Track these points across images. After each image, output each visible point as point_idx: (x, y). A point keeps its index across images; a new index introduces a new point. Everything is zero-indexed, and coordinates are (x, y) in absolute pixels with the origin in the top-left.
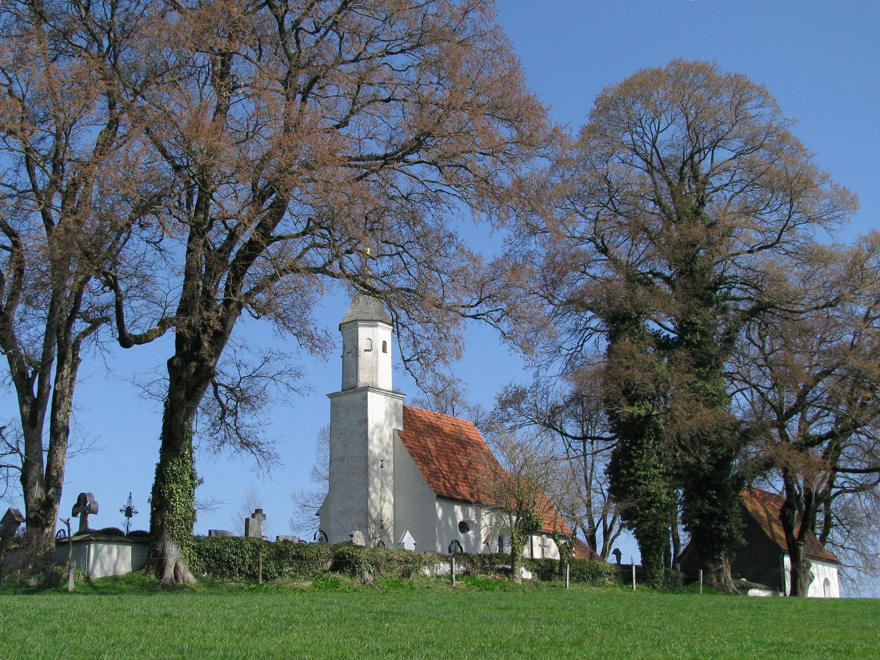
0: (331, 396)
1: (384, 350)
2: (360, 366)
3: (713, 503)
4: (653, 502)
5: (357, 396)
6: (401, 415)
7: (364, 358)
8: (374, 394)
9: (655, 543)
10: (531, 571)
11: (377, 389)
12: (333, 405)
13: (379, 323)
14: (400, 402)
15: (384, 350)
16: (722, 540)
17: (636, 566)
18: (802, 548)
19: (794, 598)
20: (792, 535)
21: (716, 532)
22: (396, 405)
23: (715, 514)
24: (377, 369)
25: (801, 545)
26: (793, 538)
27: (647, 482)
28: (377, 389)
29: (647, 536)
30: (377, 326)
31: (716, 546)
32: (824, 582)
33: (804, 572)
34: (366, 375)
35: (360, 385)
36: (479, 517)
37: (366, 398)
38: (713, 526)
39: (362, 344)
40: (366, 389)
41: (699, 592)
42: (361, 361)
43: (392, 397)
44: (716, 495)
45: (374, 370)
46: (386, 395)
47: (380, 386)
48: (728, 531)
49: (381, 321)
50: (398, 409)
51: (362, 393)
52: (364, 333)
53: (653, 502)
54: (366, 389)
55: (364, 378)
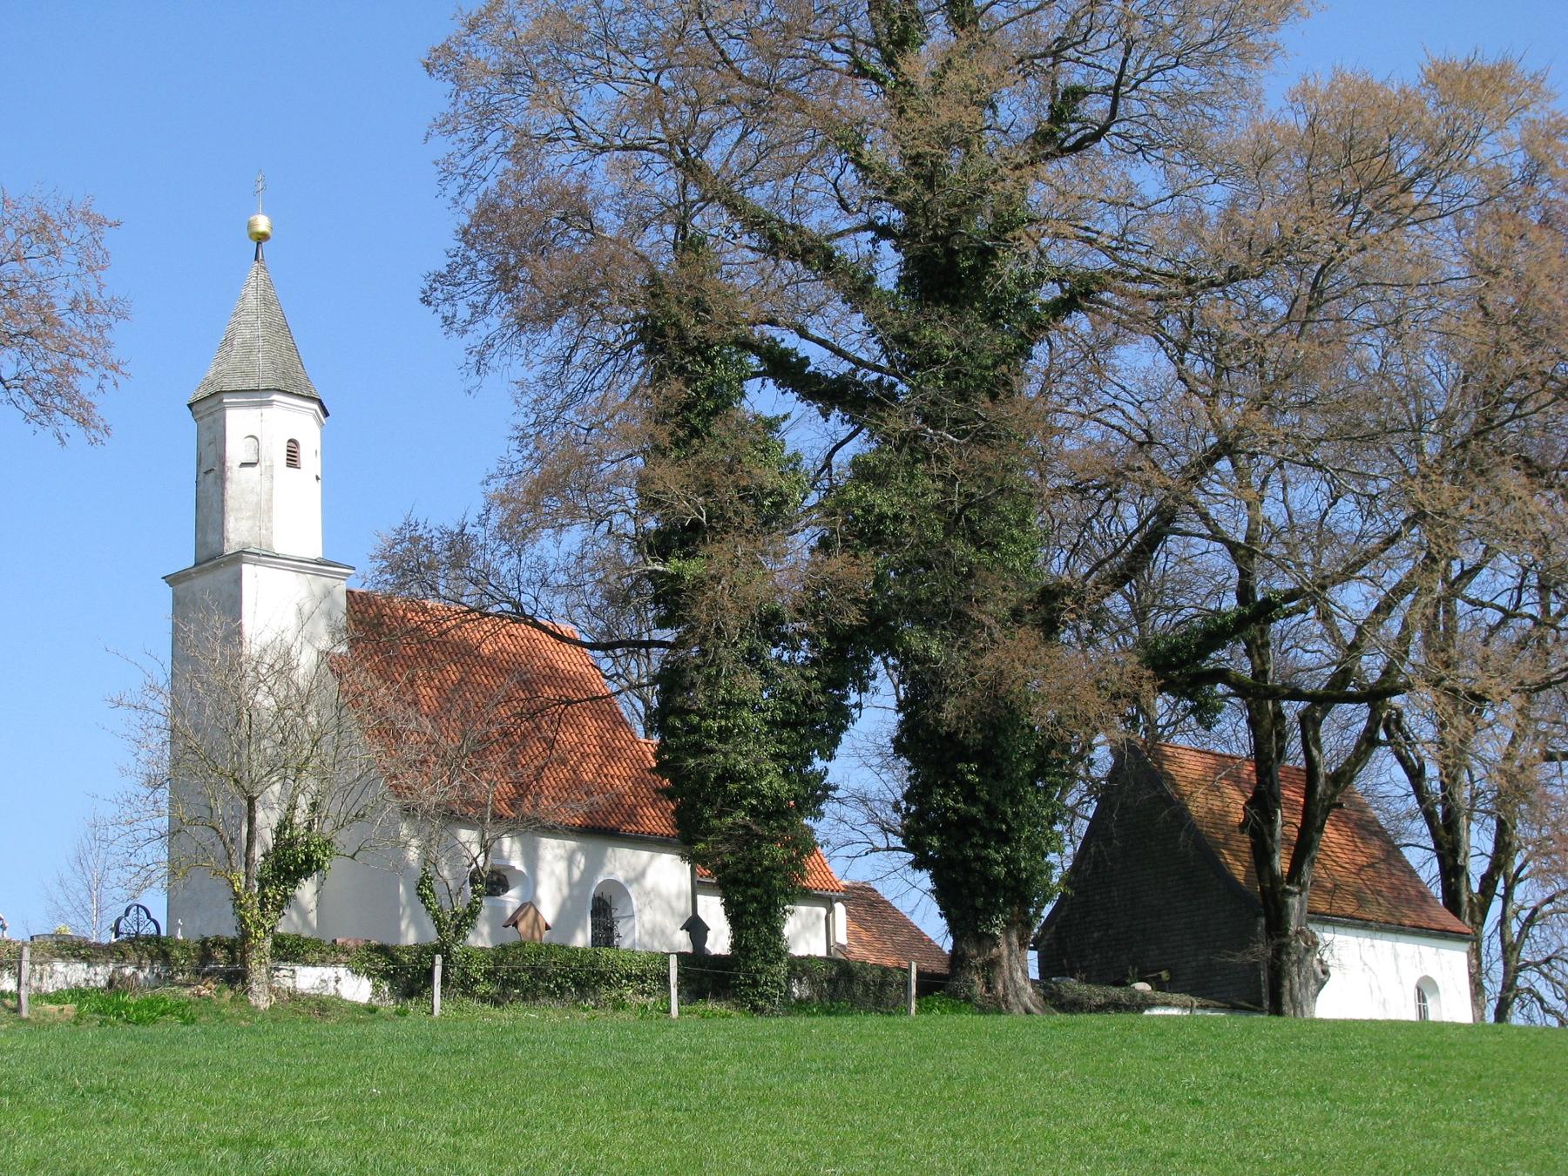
0: (173, 580)
1: (293, 459)
2: (230, 503)
3: (970, 795)
4: (743, 794)
5: (224, 574)
6: (341, 616)
7: (239, 483)
8: (261, 570)
9: (754, 898)
10: (370, 976)
11: (269, 558)
12: (177, 601)
13: (276, 397)
14: (342, 587)
15: (293, 459)
16: (994, 885)
17: (680, 956)
18: (1294, 902)
19: (1500, 1026)
20: (1272, 869)
21: (977, 866)
22: (328, 593)
23: (974, 821)
24: (270, 509)
25: (1291, 893)
26: (1274, 879)
27: (729, 747)
28: (269, 558)
29: (735, 881)
30: (269, 403)
31: (980, 902)
32: (1369, 978)
33: (1300, 961)
34: (245, 525)
35: (230, 548)
36: (532, 858)
37: (238, 580)
38: (970, 853)
39: (236, 450)
40: (238, 558)
41: (908, 1012)
42: (232, 489)
43: (318, 573)
44: (977, 773)
45: (263, 511)
46: (299, 571)
47: (279, 549)
48: (1008, 861)
49: (279, 391)
50: (335, 603)
51: (232, 569)
52: (239, 422)
53: (743, 794)
54: (238, 558)
55: (238, 531)
